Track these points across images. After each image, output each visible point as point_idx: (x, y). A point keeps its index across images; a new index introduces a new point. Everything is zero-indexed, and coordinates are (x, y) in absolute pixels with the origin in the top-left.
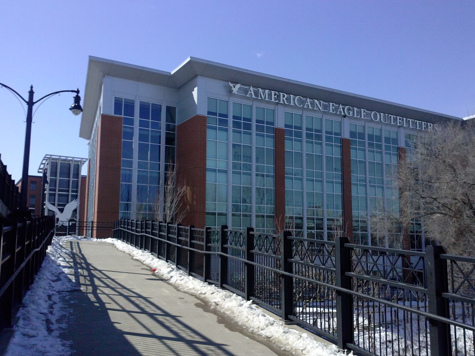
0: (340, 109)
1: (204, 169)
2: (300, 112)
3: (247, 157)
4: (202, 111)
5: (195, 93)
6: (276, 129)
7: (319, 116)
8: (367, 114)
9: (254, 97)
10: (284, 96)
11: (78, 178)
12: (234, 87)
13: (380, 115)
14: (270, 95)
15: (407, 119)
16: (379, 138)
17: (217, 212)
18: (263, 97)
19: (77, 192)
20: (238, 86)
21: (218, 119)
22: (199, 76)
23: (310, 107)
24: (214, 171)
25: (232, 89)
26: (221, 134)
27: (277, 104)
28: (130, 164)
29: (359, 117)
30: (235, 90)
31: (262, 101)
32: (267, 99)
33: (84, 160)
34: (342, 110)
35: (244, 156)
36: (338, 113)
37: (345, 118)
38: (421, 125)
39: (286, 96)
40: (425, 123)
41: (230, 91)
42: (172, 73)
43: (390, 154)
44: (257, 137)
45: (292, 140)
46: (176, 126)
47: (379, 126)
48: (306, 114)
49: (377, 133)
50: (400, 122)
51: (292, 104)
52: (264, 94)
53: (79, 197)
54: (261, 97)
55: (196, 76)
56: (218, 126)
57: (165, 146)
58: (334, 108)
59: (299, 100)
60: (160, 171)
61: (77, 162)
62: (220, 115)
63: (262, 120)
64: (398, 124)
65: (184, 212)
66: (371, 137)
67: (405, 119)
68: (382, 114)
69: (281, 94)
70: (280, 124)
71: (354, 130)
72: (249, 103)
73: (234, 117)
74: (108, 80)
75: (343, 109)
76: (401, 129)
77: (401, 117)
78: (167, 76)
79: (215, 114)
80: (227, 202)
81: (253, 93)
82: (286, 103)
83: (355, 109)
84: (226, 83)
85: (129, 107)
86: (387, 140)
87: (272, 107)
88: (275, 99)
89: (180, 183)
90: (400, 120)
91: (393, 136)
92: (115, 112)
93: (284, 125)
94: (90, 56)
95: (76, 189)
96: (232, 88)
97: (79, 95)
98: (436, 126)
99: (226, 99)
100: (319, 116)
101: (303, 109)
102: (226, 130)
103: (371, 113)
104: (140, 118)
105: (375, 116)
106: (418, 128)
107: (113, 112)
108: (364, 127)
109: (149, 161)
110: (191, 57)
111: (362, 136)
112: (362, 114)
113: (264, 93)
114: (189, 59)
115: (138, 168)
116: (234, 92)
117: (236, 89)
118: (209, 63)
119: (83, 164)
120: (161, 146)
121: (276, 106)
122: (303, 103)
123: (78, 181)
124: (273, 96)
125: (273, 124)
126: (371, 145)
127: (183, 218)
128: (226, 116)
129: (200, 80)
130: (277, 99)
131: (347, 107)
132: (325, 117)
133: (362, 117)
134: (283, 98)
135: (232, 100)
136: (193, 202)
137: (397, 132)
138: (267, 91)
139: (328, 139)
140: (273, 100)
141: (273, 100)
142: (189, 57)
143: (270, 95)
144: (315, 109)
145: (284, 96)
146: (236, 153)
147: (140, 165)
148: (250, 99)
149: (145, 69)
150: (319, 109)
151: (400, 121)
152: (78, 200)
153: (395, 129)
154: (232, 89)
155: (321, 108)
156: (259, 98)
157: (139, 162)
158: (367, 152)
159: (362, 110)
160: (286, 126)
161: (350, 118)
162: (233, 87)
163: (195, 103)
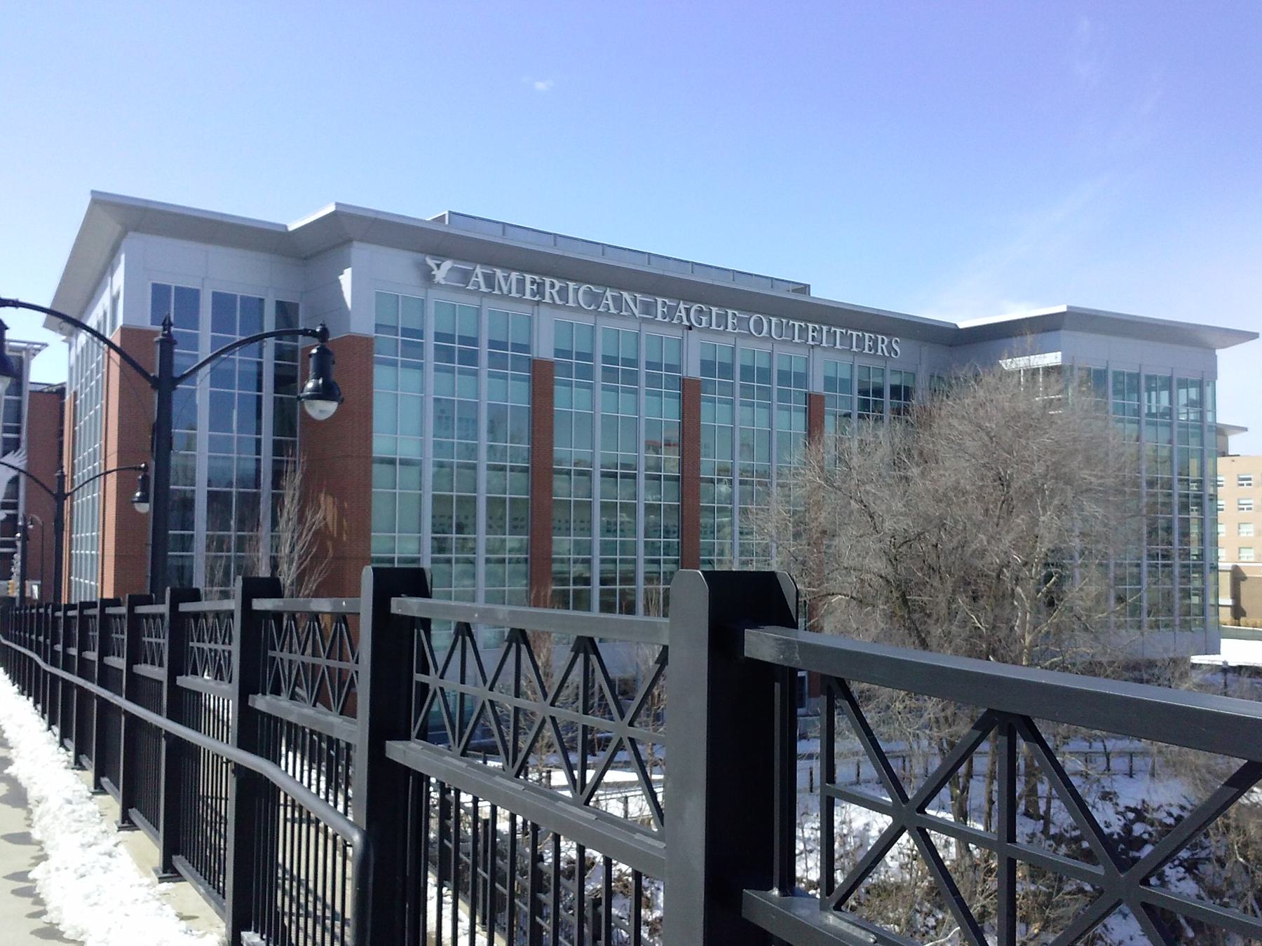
0: (680, 312)
1: (367, 459)
2: (588, 321)
3: (468, 420)
4: (361, 325)
5: (346, 279)
6: (534, 361)
7: (632, 327)
8: (740, 319)
9: (483, 289)
10: (553, 286)
11: (19, 393)
12: (438, 266)
13: (770, 322)
14: (521, 282)
15: (830, 329)
16: (765, 375)
17: (396, 556)
18: (505, 289)
19: (18, 430)
20: (447, 264)
21: (400, 342)
22: (355, 244)
23: (613, 311)
24: (392, 462)
25: (433, 273)
26: (409, 378)
27: (538, 303)
28: (190, 443)
29: (722, 328)
30: (440, 275)
31: (505, 297)
32: (514, 294)
33: (36, 346)
34: (683, 314)
35: (460, 419)
36: (674, 322)
37: (690, 331)
38: (860, 340)
39: (558, 284)
40: (870, 337)
41: (428, 276)
42: (292, 227)
43: (789, 409)
44: (492, 379)
45: (570, 384)
46: (300, 348)
47: (767, 347)
48: (603, 324)
49: (760, 362)
50: (813, 336)
51: (571, 304)
52: (507, 280)
53: (23, 445)
54: (500, 289)
55: (348, 241)
56: (400, 358)
57: (272, 398)
58: (665, 310)
59: (589, 293)
60: (262, 457)
61: (17, 352)
62: (406, 332)
63: (503, 340)
64: (810, 342)
65: (321, 568)
66: (747, 372)
67: (825, 328)
68: (774, 320)
69: (548, 281)
70: (544, 350)
71: (709, 358)
72: (474, 302)
73: (438, 336)
74: (135, 241)
75: (688, 311)
76: (817, 350)
77: (817, 326)
78: (280, 233)
79: (394, 329)
80: (419, 553)
81: (481, 279)
82: (558, 302)
83: (714, 310)
84: (419, 256)
85: (189, 298)
86: (784, 377)
87: (526, 310)
88: (534, 295)
89: (312, 501)
90: (813, 332)
91: (797, 367)
92: (152, 320)
93: (553, 351)
94: (93, 192)
95: (16, 424)
96: (433, 270)
97: (148, 473)
98: (896, 341)
99: (419, 294)
100: (632, 327)
101: (597, 313)
102: (420, 367)
103: (750, 319)
104: (212, 331)
105: (759, 324)
106: (854, 349)
107: (149, 323)
108: (733, 350)
109: (235, 434)
110: (337, 204)
111: (727, 370)
112: (730, 320)
113: (506, 279)
114: (331, 208)
115: (210, 451)
116: (436, 280)
117: (443, 271)
118: (380, 217)
119: (34, 355)
120: (264, 399)
121: (536, 307)
122: (595, 299)
123: (19, 403)
124: (528, 286)
125: (526, 348)
126: (747, 391)
127: (320, 579)
128: (419, 334)
129: (360, 251)
130: (538, 293)
131: (696, 307)
132: (647, 330)
133: (730, 329)
134: (552, 291)
135: (434, 296)
136: (340, 534)
137: (807, 360)
138: (514, 275)
139: (653, 380)
140: (528, 296)
141: (528, 296)
142: (334, 203)
143: (521, 282)
144: (624, 313)
145: (553, 286)
146: (443, 411)
147: (214, 444)
148: (476, 292)
149: (225, 220)
150: (634, 314)
151: (815, 334)
152: (24, 452)
153: (803, 353)
154: (433, 273)
155: (636, 312)
156: (497, 292)
157: (211, 437)
158: (737, 407)
159: (730, 312)
160: (558, 352)
161: (700, 330)
162: (434, 267)
163: (346, 306)
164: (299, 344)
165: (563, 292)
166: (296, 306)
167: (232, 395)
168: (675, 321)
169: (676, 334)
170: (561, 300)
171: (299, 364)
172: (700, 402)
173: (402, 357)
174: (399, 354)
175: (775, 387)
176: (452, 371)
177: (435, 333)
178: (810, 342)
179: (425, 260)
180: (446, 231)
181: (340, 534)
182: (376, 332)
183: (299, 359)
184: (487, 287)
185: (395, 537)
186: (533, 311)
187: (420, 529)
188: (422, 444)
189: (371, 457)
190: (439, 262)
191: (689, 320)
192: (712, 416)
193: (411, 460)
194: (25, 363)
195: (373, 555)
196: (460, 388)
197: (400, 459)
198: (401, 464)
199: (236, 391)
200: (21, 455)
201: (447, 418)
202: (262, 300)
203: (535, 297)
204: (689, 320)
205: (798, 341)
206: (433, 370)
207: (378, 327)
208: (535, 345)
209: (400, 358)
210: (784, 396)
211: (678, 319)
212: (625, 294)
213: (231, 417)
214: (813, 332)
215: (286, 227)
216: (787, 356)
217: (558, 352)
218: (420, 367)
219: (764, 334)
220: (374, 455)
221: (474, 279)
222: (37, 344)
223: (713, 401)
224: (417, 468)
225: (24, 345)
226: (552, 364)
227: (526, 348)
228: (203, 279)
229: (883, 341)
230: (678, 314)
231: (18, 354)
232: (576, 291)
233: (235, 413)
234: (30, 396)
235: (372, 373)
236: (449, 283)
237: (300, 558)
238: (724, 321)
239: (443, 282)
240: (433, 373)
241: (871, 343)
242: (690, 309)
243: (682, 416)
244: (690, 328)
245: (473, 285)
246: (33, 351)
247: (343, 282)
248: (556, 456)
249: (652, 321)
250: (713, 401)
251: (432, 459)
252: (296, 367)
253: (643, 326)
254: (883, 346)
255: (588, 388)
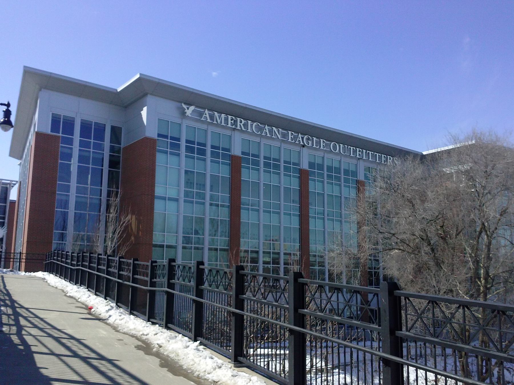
0: (299, 138)
2: (258, 140)
3: (200, 185)
4: (152, 133)
5: (144, 113)
7: (277, 144)
8: (326, 144)
9: (209, 120)
10: (241, 122)
12: (188, 108)
13: (340, 146)
14: (226, 120)
16: (338, 170)
18: (219, 121)
20: (192, 108)
22: (149, 96)
23: (268, 135)
25: (185, 111)
28: (67, 188)
29: (318, 147)
31: (217, 125)
32: (223, 124)
33: (13, 182)
34: (301, 139)
35: (197, 184)
36: (297, 142)
38: (380, 158)
39: (243, 121)
41: (183, 113)
42: (119, 90)
43: (349, 187)
47: (338, 158)
48: (264, 141)
49: (336, 164)
50: (359, 154)
51: (249, 130)
53: (6, 225)
54: (217, 121)
55: (145, 95)
61: (5, 185)
62: (172, 138)
64: (358, 156)
66: (330, 169)
70: (237, 151)
72: (204, 127)
74: (45, 94)
75: (303, 138)
77: (361, 149)
81: (208, 116)
82: (243, 129)
83: (315, 138)
84: (179, 104)
86: (346, 172)
87: (228, 133)
88: (232, 125)
91: (352, 168)
94: (25, 67)
95: (3, 216)
96: (185, 110)
99: (178, 121)
100: (277, 144)
101: (261, 136)
102: (178, 155)
103: (330, 144)
105: (335, 147)
109: (89, 186)
110: (140, 74)
111: (321, 167)
113: (220, 117)
114: (138, 76)
116: (187, 114)
117: (190, 111)
119: (13, 187)
121: (233, 132)
122: (261, 129)
123: (5, 206)
126: (330, 177)
129: (150, 99)
131: (306, 137)
132: (284, 146)
133: (322, 148)
135: (185, 123)
136: (138, 232)
139: (286, 169)
140: (229, 125)
141: (229, 125)
142: (139, 74)
143: (226, 120)
150: (278, 138)
152: (6, 227)
153: (354, 161)
154: (185, 111)
155: (279, 137)
156: (215, 122)
159: (322, 140)
160: (243, 153)
162: (186, 109)
164: (122, 146)
165: (245, 125)
166: (121, 128)
167: (89, 167)
168: (297, 142)
169: (297, 149)
170: (245, 129)
171: (121, 155)
172: (308, 180)
173: (170, 140)
174: (169, 148)
175: (343, 176)
176: (193, 158)
177: (186, 140)
178: (358, 156)
179: (182, 106)
180: (192, 91)
181: (138, 232)
182: (158, 137)
183: (121, 153)
184: (211, 120)
185: (165, 235)
186: (232, 133)
187: (179, 186)
188: (179, 191)
189: (154, 195)
190: (188, 107)
191: (303, 142)
192: (314, 187)
193: (172, 245)
194: (8, 190)
195: (153, 243)
196: (197, 167)
197: (166, 245)
198: (168, 200)
199: (91, 166)
200: (4, 229)
201: (191, 183)
202: (105, 125)
203: (233, 126)
204: (303, 142)
205: (353, 156)
206: (184, 157)
207: (159, 135)
208: (233, 150)
209: (169, 150)
210: (346, 181)
211: (298, 142)
212: (274, 128)
213: (88, 178)
214: (359, 152)
215: (117, 90)
216: (347, 163)
217: (243, 153)
218: (178, 155)
219: (337, 151)
220: (155, 195)
221: (204, 115)
222: (15, 181)
223: (314, 180)
224: (174, 249)
225: (9, 182)
226: (240, 157)
227: (229, 150)
228: (77, 113)
229: (390, 159)
230: (298, 139)
231: (6, 186)
232: (252, 125)
233: (90, 176)
234: (10, 204)
235: (155, 156)
236: (193, 117)
237: (117, 239)
238: (319, 144)
239: (190, 116)
240: (184, 158)
241: (385, 159)
242: (304, 137)
243: (300, 186)
244: (304, 146)
245: (204, 119)
246: (13, 185)
247: (142, 114)
248: (242, 201)
249: (287, 142)
250: (314, 180)
251: (183, 198)
252: (120, 156)
253: (283, 144)
254: (390, 161)
255: (257, 170)
